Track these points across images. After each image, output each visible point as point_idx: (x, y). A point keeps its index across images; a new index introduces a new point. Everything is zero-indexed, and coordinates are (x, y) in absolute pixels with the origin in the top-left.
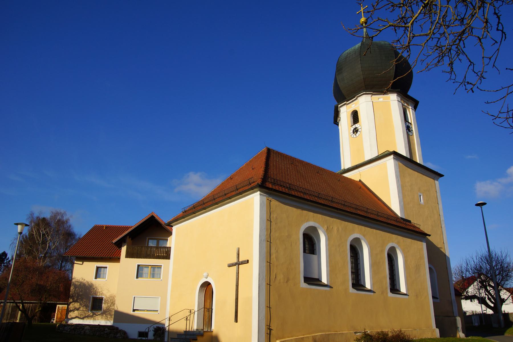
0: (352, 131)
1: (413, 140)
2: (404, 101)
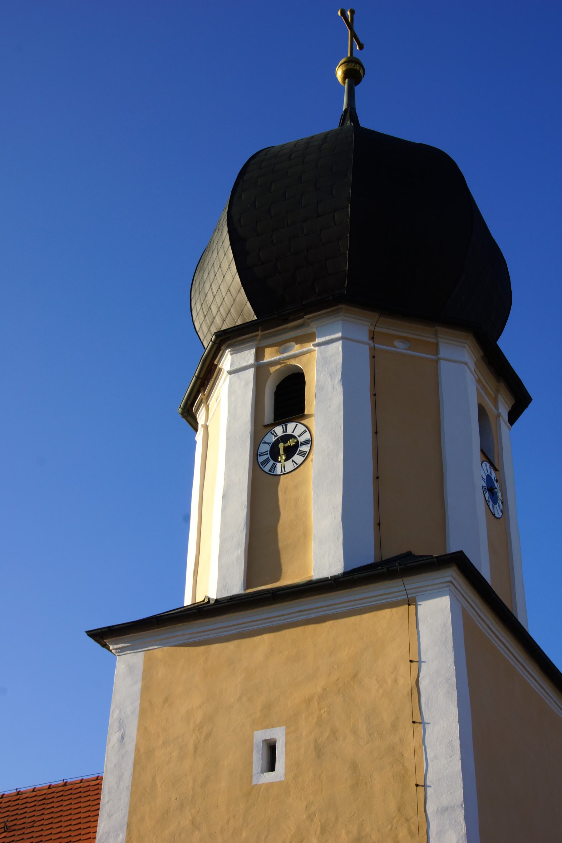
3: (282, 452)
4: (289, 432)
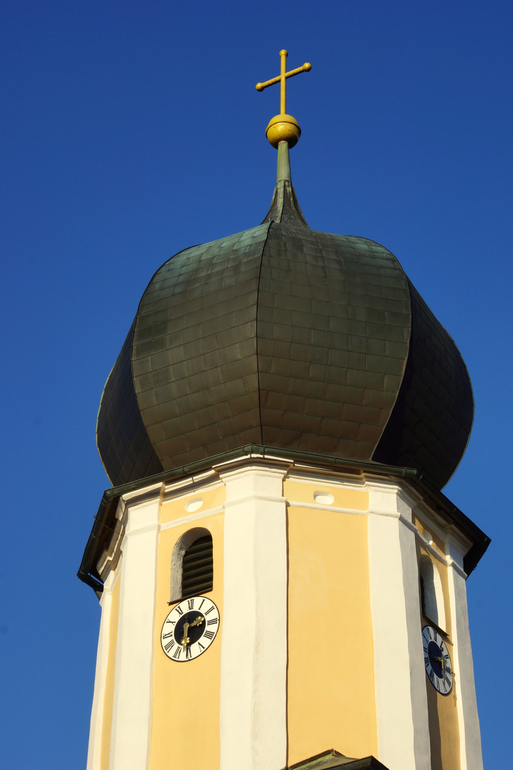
0: (171, 628)
1: (452, 718)
2: (426, 528)
3: (186, 633)
4: (196, 609)
